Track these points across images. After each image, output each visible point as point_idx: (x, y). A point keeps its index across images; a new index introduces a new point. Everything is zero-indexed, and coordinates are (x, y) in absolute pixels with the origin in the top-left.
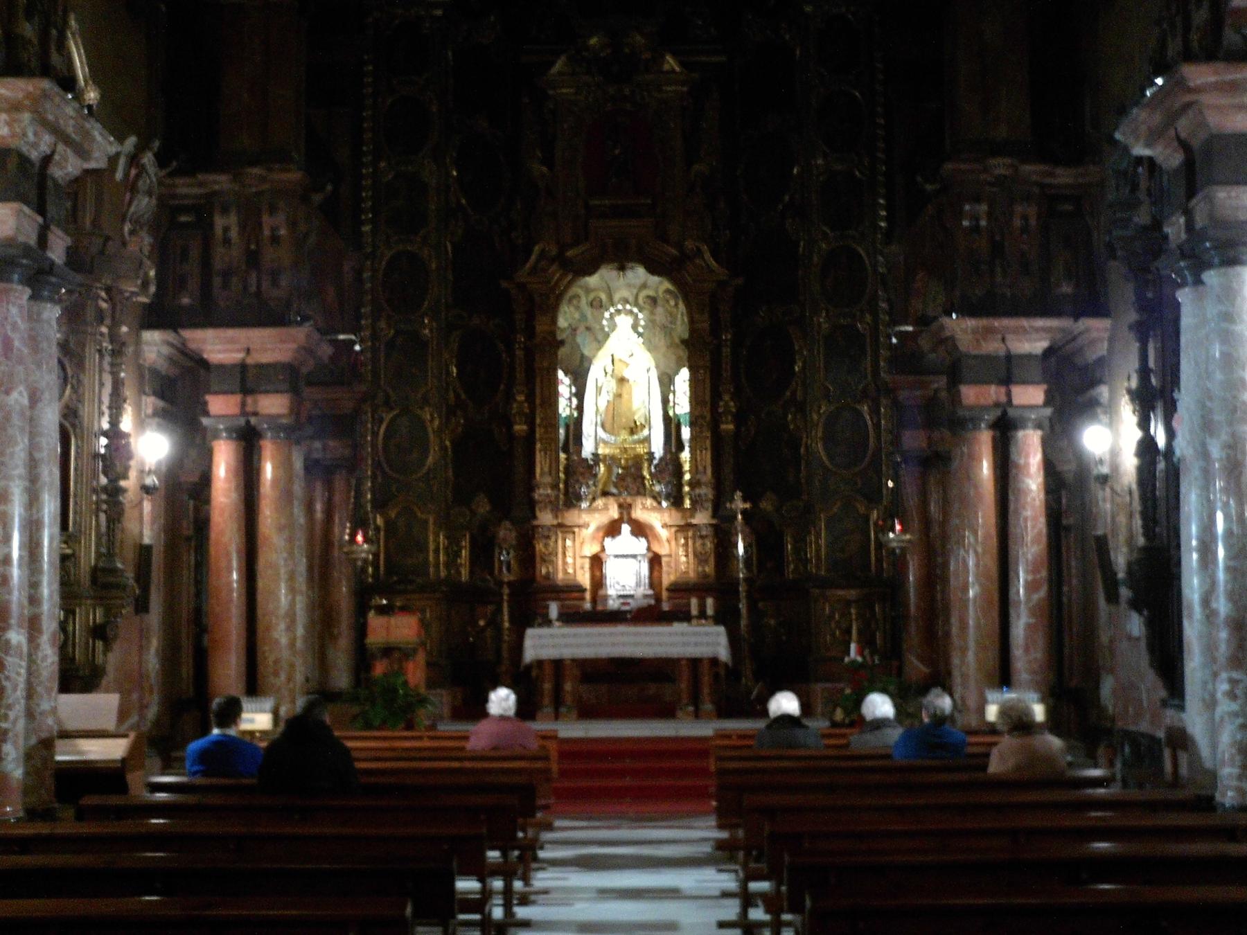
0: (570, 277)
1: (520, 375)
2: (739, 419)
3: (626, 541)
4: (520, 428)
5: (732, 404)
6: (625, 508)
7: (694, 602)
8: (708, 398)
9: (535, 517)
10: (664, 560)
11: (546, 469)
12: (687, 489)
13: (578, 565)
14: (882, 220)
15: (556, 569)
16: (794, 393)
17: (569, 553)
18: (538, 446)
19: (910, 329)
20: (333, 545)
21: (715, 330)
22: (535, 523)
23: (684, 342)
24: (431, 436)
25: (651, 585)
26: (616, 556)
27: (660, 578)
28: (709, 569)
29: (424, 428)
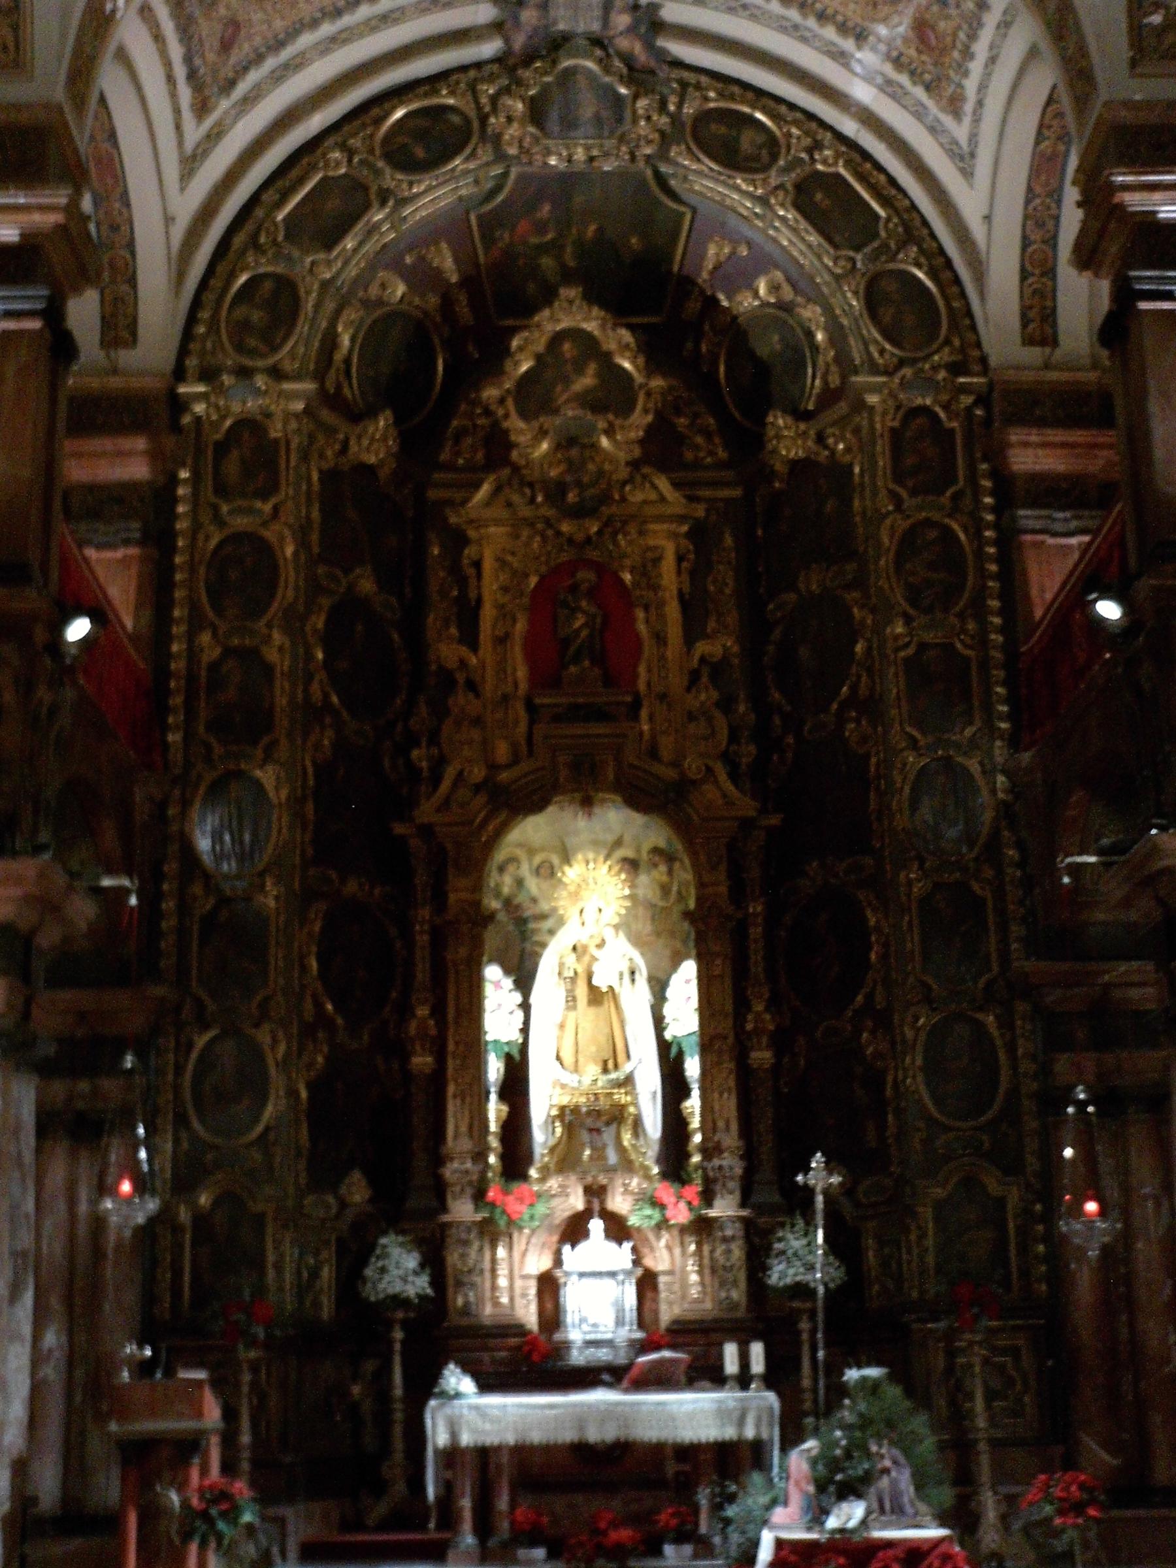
0: (503, 816)
1: (422, 973)
2: (781, 1042)
3: (597, 1250)
4: (422, 1061)
5: (768, 1017)
6: (596, 1192)
7: (730, 1351)
8: (729, 1007)
9: (444, 1209)
10: (662, 1279)
11: (464, 1129)
12: (696, 1159)
13: (518, 1291)
14: (1001, 719)
15: (480, 1300)
16: (870, 997)
17: (503, 1271)
18: (451, 1089)
19: (1092, 859)
20: (105, 1256)
21: (738, 893)
22: (446, 1218)
23: (687, 915)
24: (272, 1070)
25: (641, 1324)
26: (582, 1275)
27: (656, 1312)
28: (738, 1294)
29: (261, 1058)
